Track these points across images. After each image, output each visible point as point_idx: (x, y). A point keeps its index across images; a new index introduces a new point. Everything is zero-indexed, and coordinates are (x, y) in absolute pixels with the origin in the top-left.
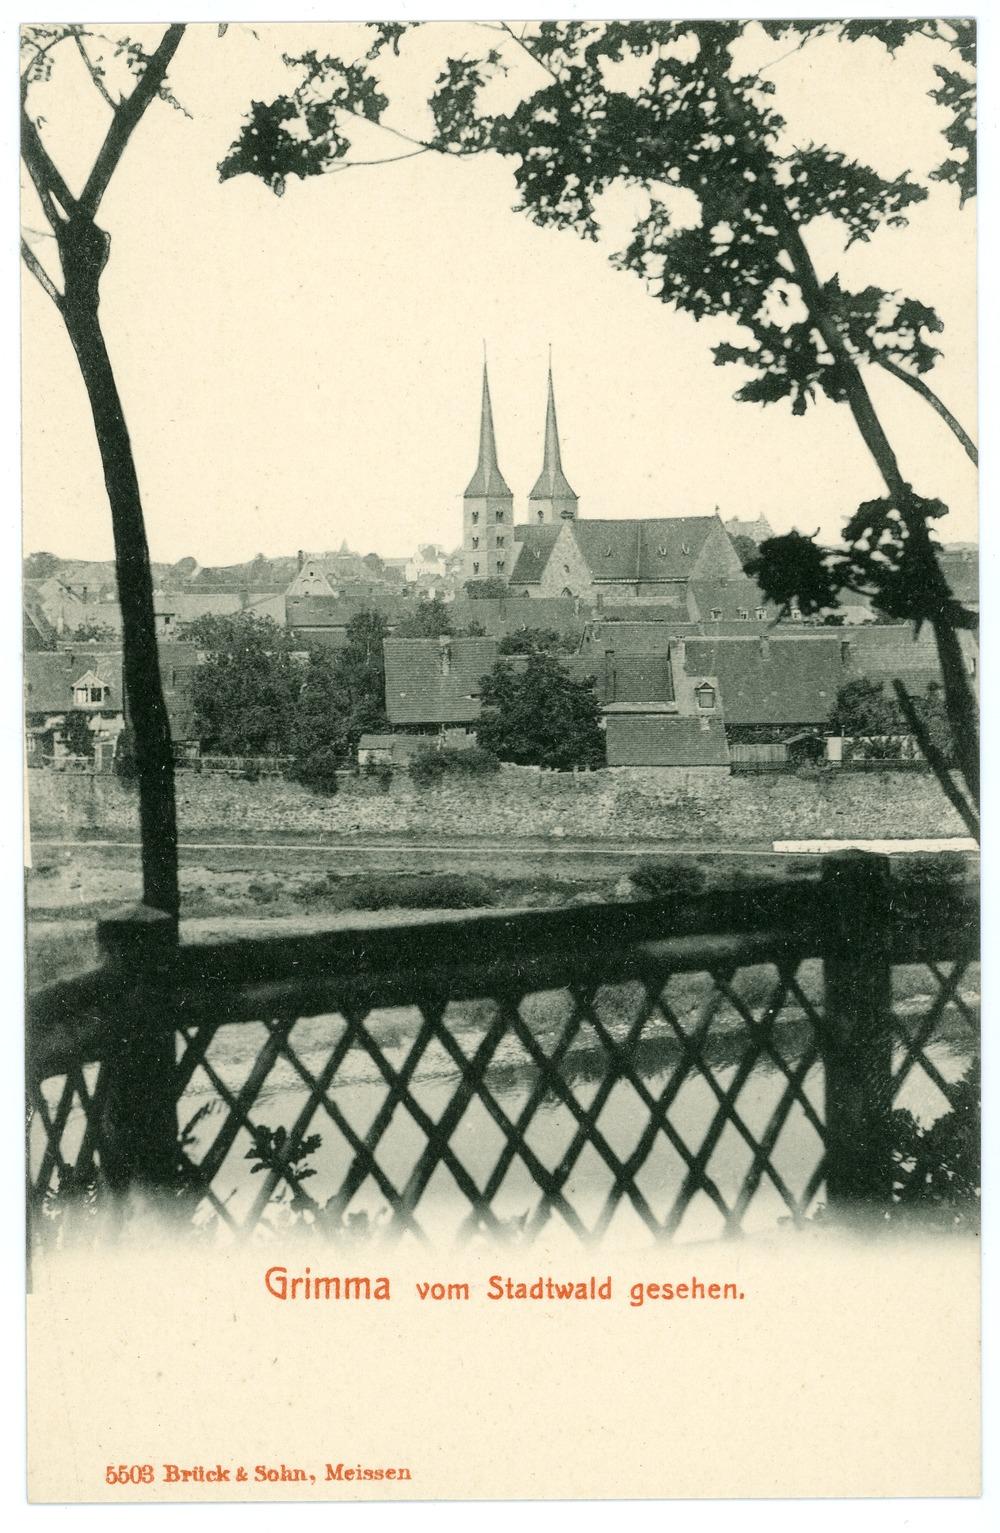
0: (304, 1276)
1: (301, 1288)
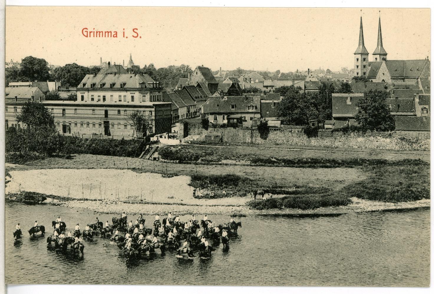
0: (93, 31)
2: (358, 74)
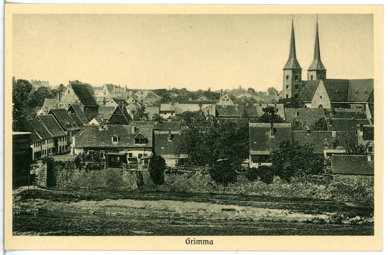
0: (194, 240)
1: (193, 242)
2: (287, 96)
